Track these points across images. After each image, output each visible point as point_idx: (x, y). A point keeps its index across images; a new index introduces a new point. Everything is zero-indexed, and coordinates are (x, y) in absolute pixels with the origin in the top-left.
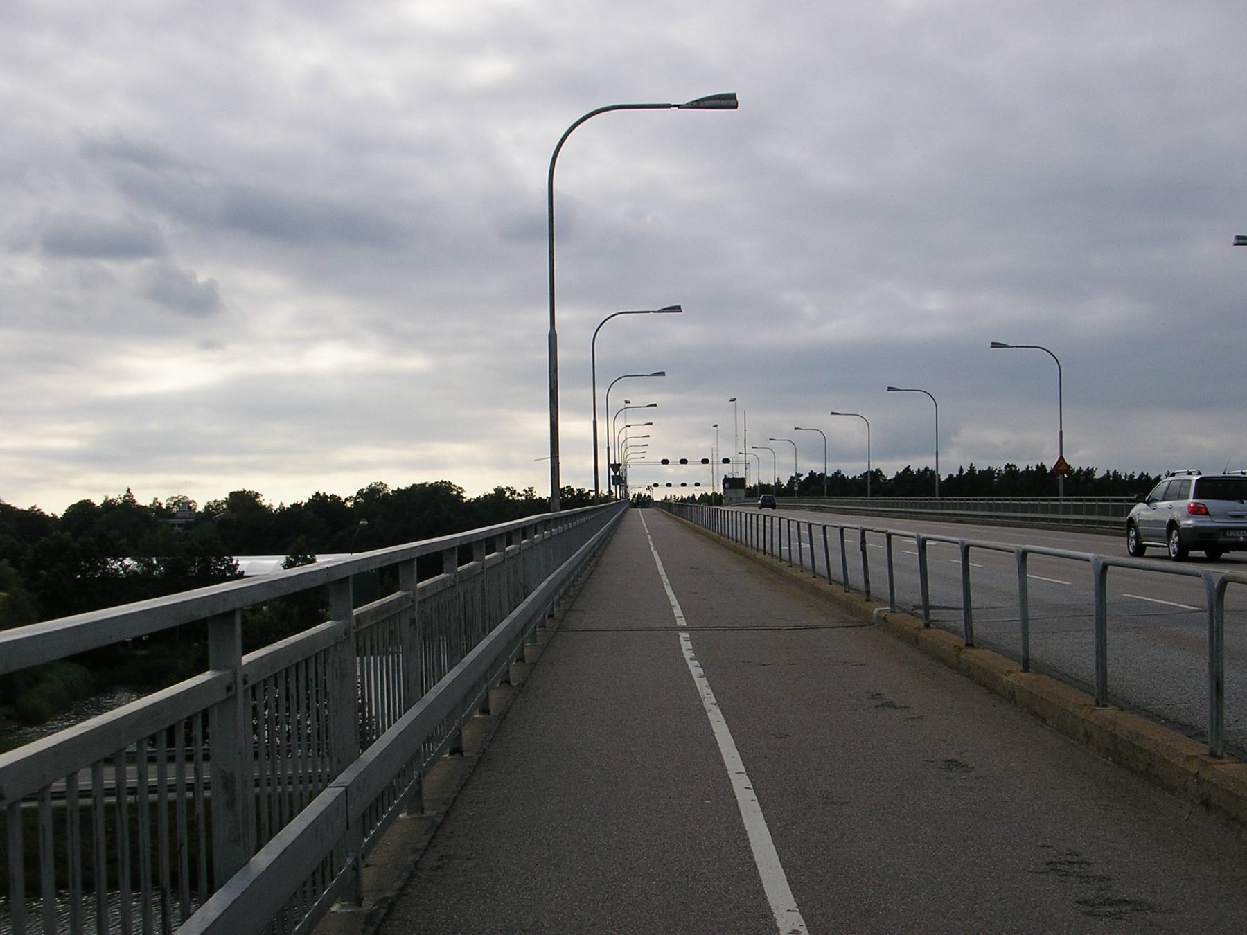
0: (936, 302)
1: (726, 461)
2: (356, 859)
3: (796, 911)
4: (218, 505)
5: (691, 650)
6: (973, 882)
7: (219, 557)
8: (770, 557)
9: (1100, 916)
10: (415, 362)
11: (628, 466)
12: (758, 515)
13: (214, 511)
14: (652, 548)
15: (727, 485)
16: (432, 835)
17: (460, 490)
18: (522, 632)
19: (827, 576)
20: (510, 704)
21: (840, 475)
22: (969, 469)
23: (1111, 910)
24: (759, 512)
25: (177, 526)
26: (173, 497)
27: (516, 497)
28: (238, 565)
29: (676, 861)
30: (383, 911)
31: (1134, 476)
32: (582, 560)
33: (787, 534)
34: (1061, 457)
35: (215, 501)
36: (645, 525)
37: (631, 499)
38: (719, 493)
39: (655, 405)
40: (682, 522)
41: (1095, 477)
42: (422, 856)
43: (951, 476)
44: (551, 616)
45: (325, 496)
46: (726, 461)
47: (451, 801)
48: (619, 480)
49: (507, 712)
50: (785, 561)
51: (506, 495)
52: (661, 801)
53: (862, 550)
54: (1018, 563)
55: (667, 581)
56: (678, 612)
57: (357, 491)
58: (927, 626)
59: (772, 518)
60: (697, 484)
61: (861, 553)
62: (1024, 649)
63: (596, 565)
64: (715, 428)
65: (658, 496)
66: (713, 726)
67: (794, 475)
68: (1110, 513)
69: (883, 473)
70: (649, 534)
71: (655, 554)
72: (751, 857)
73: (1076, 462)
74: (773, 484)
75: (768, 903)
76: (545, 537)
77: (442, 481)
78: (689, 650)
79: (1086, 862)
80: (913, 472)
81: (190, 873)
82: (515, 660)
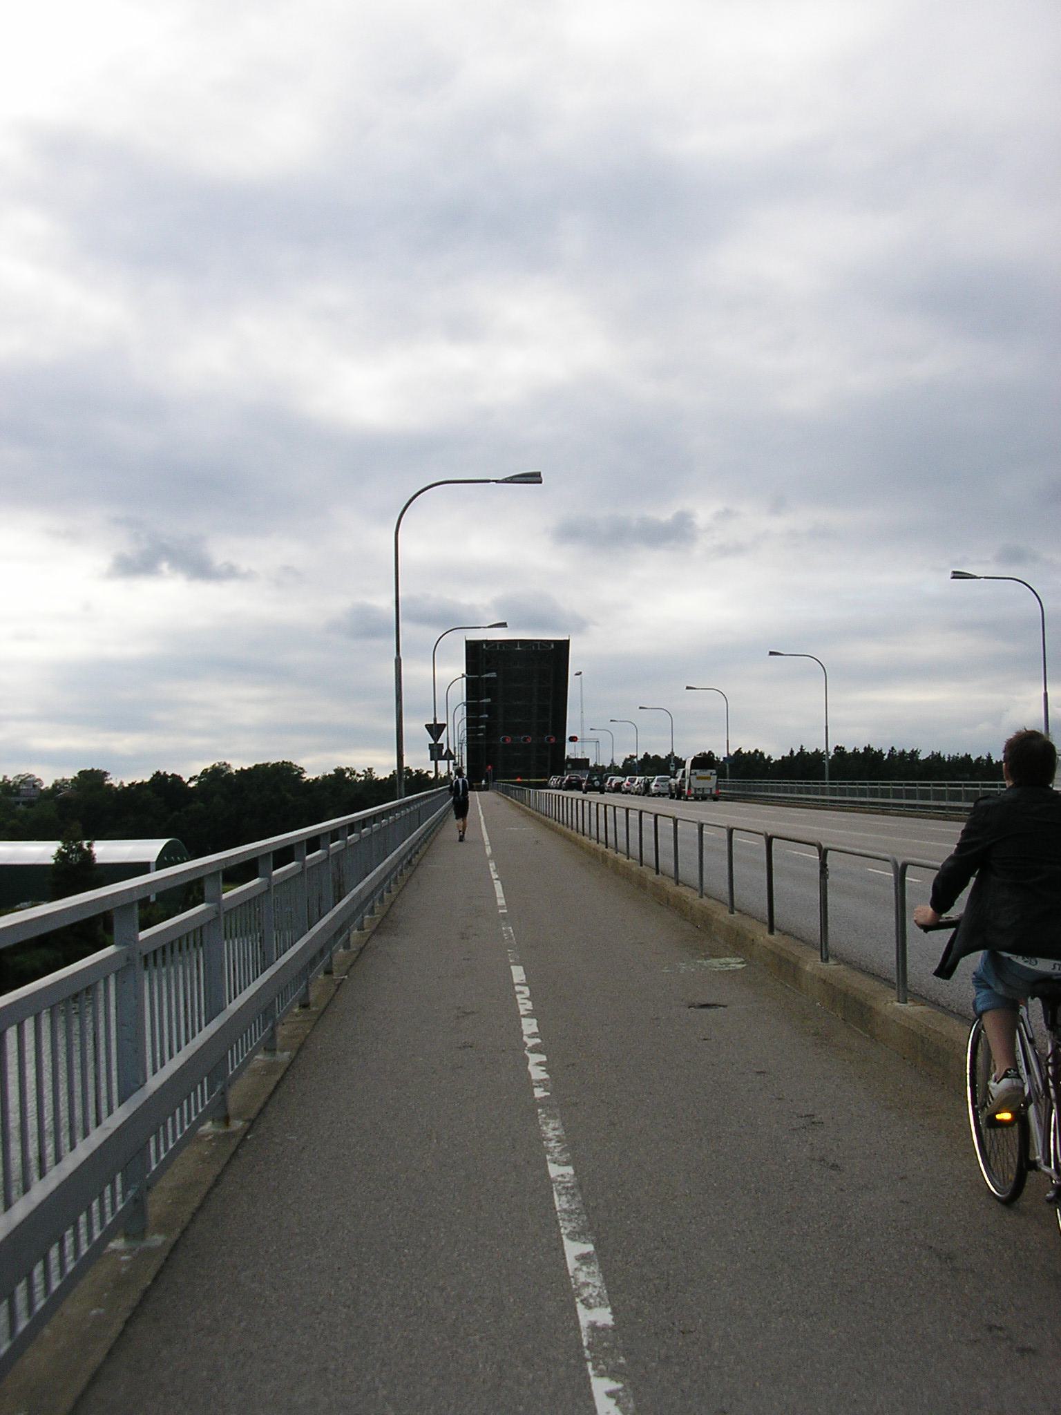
17: (301, 771)
24: (584, 796)
25: (21, 804)
26: (19, 776)
41: (919, 758)
45: (165, 776)
68: (891, 796)
81: (155, 1041)
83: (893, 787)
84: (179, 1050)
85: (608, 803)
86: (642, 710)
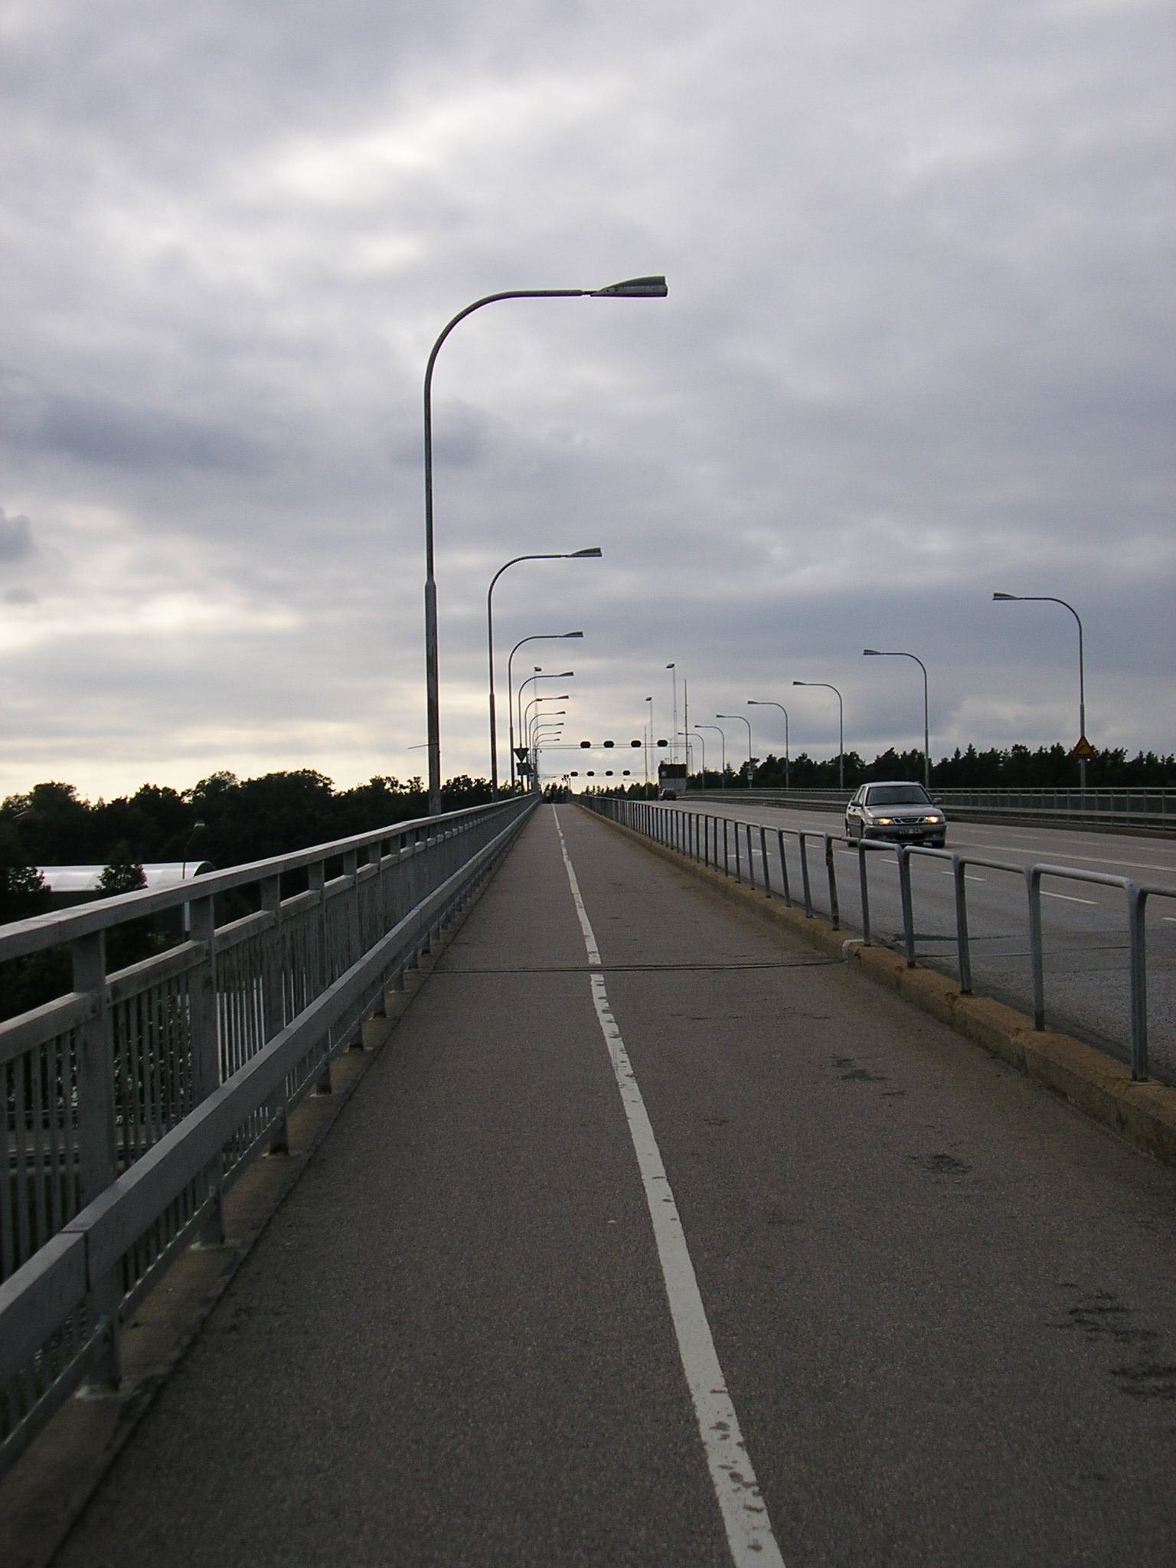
0: (937, 542)
1: (663, 743)
2: (111, 1326)
3: (724, 1392)
4: (20, 801)
5: (604, 998)
6: (968, 1342)
7: (20, 866)
8: (713, 870)
9: (1142, 1393)
10: (280, 619)
11: (539, 751)
12: (698, 816)
13: (15, 809)
14: (565, 857)
15: (663, 774)
16: (231, 1276)
18: (382, 977)
19: (784, 894)
20: (359, 1078)
21: (805, 761)
22: (967, 751)
23: (1160, 1383)
27: (398, 790)
28: (43, 878)
29: (562, 1314)
30: (148, 1398)
31: (1173, 759)
32: (472, 875)
33: (734, 837)
34: (1083, 738)
35: (16, 797)
36: (559, 828)
37: (543, 791)
38: (654, 784)
39: (571, 674)
40: (609, 824)
42: (213, 1310)
43: (944, 761)
44: (426, 952)
45: (157, 790)
46: (663, 743)
47: (264, 1223)
48: (527, 769)
49: (354, 1091)
50: (731, 874)
51: (386, 787)
52: (549, 1222)
53: (827, 864)
54: (1028, 884)
55: (581, 901)
56: (591, 945)
57: (197, 783)
58: (911, 965)
59: (716, 819)
60: (627, 773)
61: (827, 868)
62: (1036, 998)
63: (492, 880)
64: (649, 702)
65: (577, 787)
66: (626, 1108)
67: (748, 761)
69: (860, 758)
70: (563, 838)
71: (569, 864)
72: (666, 1307)
73: (1102, 742)
74: (721, 771)
75: (686, 1380)
76: (447, 837)
77: (304, 770)
78: (602, 998)
79: (1123, 1310)
80: (897, 756)
82: (373, 1013)
83: (1099, 795)
84: (260, 1048)
85: (717, 816)
86: (796, 686)
